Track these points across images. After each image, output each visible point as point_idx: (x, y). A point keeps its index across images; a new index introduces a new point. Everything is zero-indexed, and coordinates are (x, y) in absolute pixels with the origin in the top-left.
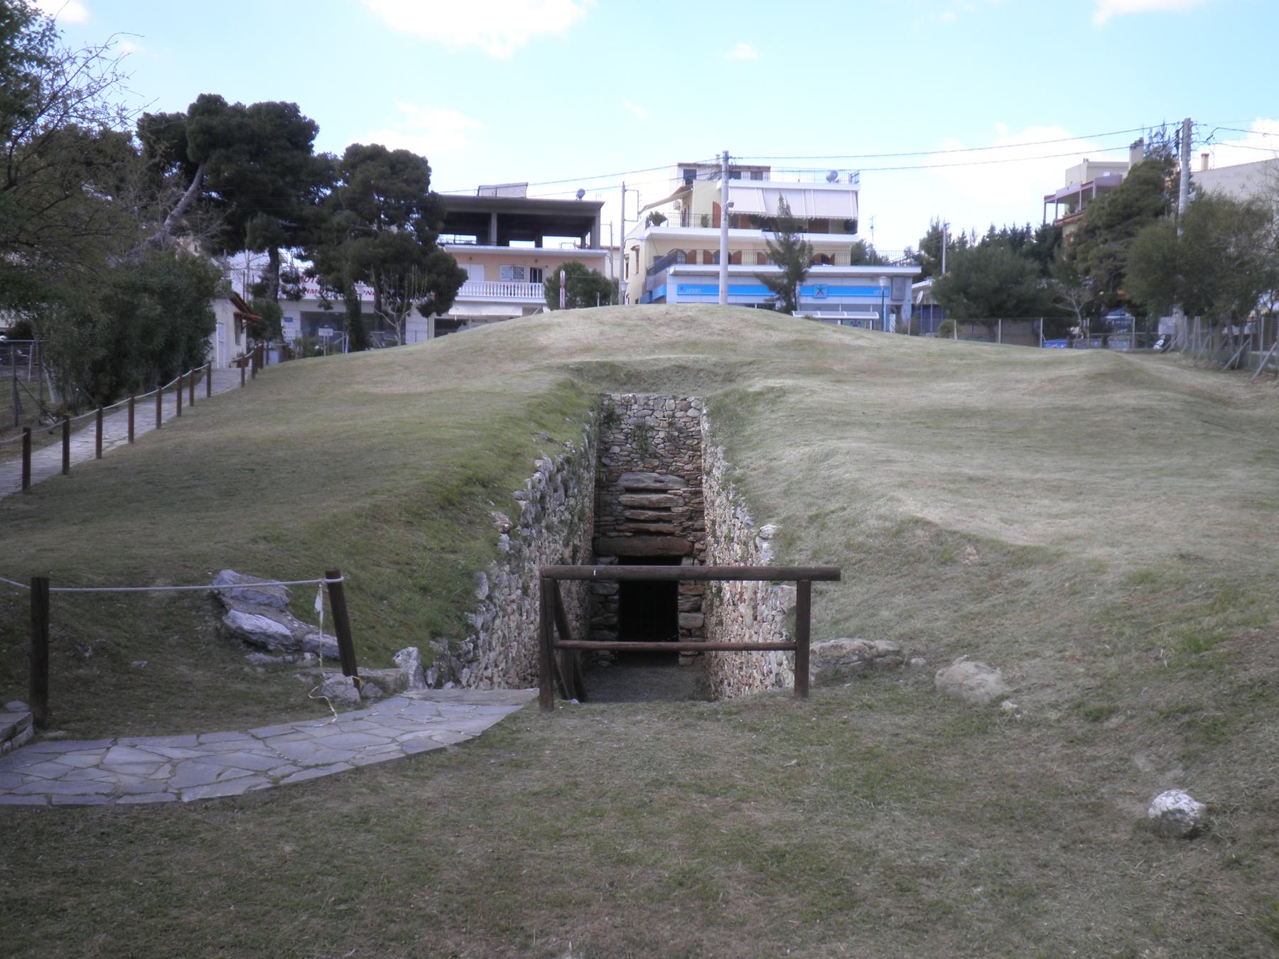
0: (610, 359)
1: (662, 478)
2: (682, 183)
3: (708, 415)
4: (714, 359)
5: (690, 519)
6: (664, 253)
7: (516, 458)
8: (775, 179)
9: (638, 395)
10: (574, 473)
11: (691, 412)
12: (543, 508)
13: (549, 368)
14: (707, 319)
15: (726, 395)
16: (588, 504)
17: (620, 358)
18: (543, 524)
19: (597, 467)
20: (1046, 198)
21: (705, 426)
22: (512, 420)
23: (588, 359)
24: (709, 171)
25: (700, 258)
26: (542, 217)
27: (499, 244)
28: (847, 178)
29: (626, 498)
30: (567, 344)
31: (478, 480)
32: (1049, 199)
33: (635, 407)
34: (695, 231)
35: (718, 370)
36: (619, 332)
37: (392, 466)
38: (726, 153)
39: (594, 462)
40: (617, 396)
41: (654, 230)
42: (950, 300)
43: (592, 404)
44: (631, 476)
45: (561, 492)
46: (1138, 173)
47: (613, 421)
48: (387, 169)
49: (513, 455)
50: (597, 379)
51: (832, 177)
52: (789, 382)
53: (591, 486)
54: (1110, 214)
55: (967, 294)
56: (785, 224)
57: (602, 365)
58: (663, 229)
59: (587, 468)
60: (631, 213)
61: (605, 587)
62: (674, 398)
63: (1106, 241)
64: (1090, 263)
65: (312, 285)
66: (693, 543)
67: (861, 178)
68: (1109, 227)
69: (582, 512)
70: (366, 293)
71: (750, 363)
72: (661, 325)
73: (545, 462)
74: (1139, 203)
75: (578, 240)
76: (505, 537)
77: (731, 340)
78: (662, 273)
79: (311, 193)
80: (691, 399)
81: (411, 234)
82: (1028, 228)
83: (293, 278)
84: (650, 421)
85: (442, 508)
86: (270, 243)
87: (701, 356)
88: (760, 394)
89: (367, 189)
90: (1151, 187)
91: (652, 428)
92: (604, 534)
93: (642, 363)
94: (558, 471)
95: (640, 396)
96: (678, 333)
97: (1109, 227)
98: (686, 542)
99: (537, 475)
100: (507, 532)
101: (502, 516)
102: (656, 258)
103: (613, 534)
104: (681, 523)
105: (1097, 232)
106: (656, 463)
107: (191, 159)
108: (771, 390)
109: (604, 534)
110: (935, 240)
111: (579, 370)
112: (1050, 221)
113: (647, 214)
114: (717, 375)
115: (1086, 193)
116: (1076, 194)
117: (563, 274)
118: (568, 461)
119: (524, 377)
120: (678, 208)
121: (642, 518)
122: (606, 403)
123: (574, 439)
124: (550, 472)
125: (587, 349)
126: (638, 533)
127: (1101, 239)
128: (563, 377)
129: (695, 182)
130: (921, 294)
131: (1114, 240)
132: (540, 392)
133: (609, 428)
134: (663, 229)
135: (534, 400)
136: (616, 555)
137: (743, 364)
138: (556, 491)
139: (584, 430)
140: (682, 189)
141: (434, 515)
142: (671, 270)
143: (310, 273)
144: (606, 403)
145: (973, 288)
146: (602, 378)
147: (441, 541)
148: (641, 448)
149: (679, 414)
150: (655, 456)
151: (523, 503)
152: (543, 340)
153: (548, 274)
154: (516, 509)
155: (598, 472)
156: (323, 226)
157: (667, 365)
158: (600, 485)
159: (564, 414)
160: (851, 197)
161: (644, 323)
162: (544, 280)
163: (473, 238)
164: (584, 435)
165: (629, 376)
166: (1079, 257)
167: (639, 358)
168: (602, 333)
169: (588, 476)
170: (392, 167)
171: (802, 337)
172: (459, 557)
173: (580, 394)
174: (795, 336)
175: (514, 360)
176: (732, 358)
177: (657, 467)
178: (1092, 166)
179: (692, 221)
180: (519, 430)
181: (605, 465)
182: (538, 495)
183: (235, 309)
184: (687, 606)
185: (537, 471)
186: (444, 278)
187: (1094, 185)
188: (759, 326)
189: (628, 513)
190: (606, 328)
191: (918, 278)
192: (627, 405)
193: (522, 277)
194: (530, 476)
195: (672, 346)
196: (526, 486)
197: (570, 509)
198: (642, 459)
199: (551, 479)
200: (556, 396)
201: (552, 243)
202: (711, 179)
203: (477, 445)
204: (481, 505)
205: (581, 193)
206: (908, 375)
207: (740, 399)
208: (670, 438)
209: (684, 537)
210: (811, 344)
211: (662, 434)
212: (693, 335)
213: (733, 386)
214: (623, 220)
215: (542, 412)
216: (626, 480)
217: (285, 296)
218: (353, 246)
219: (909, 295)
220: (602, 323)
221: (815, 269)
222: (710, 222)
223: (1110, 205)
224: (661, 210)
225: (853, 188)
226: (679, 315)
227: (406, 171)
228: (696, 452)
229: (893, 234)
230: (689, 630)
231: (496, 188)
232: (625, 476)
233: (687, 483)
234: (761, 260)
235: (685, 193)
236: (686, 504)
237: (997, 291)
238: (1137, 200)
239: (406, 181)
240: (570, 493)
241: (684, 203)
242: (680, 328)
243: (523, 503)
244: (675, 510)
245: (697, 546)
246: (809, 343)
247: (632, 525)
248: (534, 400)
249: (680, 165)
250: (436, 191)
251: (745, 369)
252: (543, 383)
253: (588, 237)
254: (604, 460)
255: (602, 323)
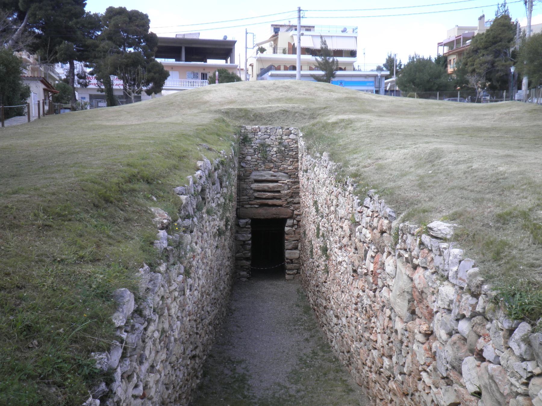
0: (244, 107)
1: (275, 174)
2: (273, 34)
3: (303, 137)
4: (303, 106)
5: (292, 197)
6: (266, 66)
7: (181, 160)
8: (317, 31)
9: (261, 127)
10: (226, 171)
11: (292, 136)
12: (203, 199)
13: (210, 112)
14: (296, 87)
15: (314, 125)
16: (234, 189)
17: (250, 106)
18: (204, 211)
19: (239, 168)
20: (438, 44)
21: (302, 143)
22: (184, 136)
23: (232, 107)
24: (286, 29)
25: (282, 68)
26: (205, 49)
27: (186, 60)
28: (352, 30)
29: (255, 186)
30: (220, 100)
31: (143, 178)
32: (440, 44)
33: (260, 133)
34: (280, 56)
35: (306, 112)
36: (248, 93)
37: (59, 166)
38: (299, 8)
39: (237, 165)
40: (249, 127)
41: (260, 55)
42: (406, 87)
43: (235, 131)
44: (258, 173)
45: (218, 184)
46: (500, 21)
47: (247, 141)
48: (127, 19)
49: (180, 157)
50: (238, 118)
51: (344, 31)
52: (352, 116)
53: (236, 179)
54: (486, 42)
55: (414, 84)
56: (324, 52)
57: (240, 110)
58: (265, 55)
59: (233, 168)
60: (250, 45)
61: (244, 236)
62: (282, 128)
63: (483, 55)
64: (475, 66)
65: (94, 81)
66: (293, 211)
67: (358, 30)
68: (486, 48)
69: (231, 195)
70: (118, 84)
71: (325, 108)
72: (271, 90)
73: (205, 163)
74: (501, 36)
75: (224, 61)
76: (162, 233)
77: (311, 97)
78: (266, 74)
79: (90, 33)
80: (291, 128)
81: (140, 52)
82: (430, 58)
83: (82, 76)
84: (268, 141)
85: (96, 206)
86: (68, 58)
87: (296, 105)
88: (336, 123)
89: (117, 29)
90: (506, 28)
91: (269, 146)
92: (243, 206)
93: (263, 109)
94: (215, 170)
95: (263, 127)
96: (281, 94)
97: (486, 48)
98: (289, 210)
99: (199, 173)
100: (165, 227)
101: (161, 212)
102: (261, 69)
103: (247, 206)
104: (286, 200)
105: (479, 51)
106: (272, 165)
107: (21, 8)
108: (342, 121)
109: (243, 206)
110: (390, 63)
111: (227, 113)
112: (441, 54)
113: (257, 48)
114: (305, 115)
115: (458, 41)
116: (453, 42)
117: (217, 73)
118: (222, 163)
119: (195, 116)
120: (271, 46)
121: (264, 197)
122: (243, 131)
123: (226, 150)
124: (209, 170)
125: (231, 102)
126: (262, 205)
127: (481, 54)
128: (217, 116)
129: (279, 33)
130: (389, 85)
131: (488, 55)
132: (204, 123)
133: (245, 146)
134: (265, 55)
135: (200, 127)
136: (250, 218)
137: (320, 109)
138: (214, 184)
139: (231, 145)
140: (273, 36)
141: (83, 215)
142: (270, 73)
143: (91, 73)
144: (243, 131)
145: (417, 80)
146: (240, 117)
147: (82, 248)
148: (263, 157)
149: (284, 137)
150: (271, 161)
151: (183, 198)
152: (206, 98)
153: (210, 75)
154: (177, 204)
155: (239, 171)
156: (97, 49)
157: (277, 110)
158: (240, 178)
159: (219, 135)
160: (354, 39)
161: (262, 89)
162: (208, 77)
163: (174, 60)
164: (231, 148)
165: (256, 116)
166: (469, 64)
167: (261, 106)
168: (239, 94)
169: (234, 173)
170: (130, 19)
171: (349, 96)
172: (100, 268)
173: (228, 125)
174: (345, 95)
175: (190, 108)
176: (313, 106)
177: (272, 168)
178: (460, 29)
179: (278, 51)
180: (188, 142)
181: (242, 167)
182: (200, 189)
183: (45, 87)
184: (290, 246)
185: (198, 169)
186: (157, 75)
187: (461, 37)
188: (325, 90)
189: (256, 194)
190: (241, 92)
191: (387, 77)
192: (255, 132)
193: (197, 77)
194: (192, 174)
195: (279, 100)
196: (188, 182)
197: (224, 196)
198: (264, 163)
199: (210, 176)
200: (214, 125)
201: (210, 62)
202: (287, 31)
203: (149, 149)
204: (141, 201)
205: (226, 37)
206: (415, 114)
207: (323, 127)
208: (279, 151)
209: (288, 207)
210: (355, 99)
211: (275, 149)
212: (290, 95)
213: (316, 121)
214: (246, 48)
215: (205, 135)
216: (255, 175)
217: (79, 86)
218: (111, 58)
219: (383, 86)
220: (239, 89)
221: (339, 73)
222: (287, 52)
223: (486, 37)
224: (264, 46)
225: (354, 35)
226: (281, 85)
227: (136, 22)
228: (296, 159)
229: (368, 62)
230: (291, 260)
231: (184, 35)
232: (254, 173)
233: (290, 177)
234: (311, 69)
235: (275, 38)
236: (289, 189)
237: (428, 81)
238: (500, 34)
239: (137, 26)
240: (224, 185)
241: (274, 43)
242: (282, 91)
243: (183, 198)
244: (283, 192)
245: (296, 212)
246: (354, 98)
247: (258, 201)
248: (200, 127)
249: (272, 25)
250: (154, 32)
251: (322, 111)
252: (206, 119)
253: (229, 60)
254: (242, 164)
255: (239, 89)
